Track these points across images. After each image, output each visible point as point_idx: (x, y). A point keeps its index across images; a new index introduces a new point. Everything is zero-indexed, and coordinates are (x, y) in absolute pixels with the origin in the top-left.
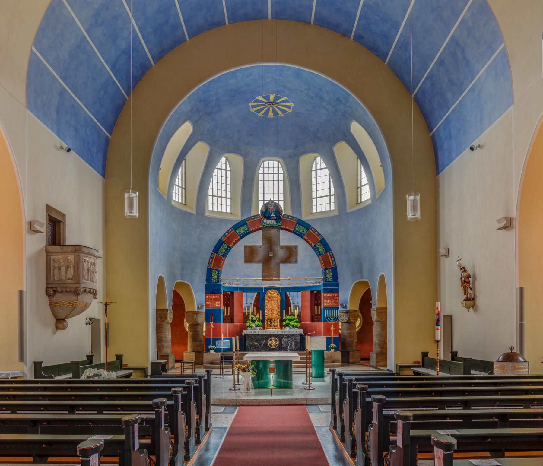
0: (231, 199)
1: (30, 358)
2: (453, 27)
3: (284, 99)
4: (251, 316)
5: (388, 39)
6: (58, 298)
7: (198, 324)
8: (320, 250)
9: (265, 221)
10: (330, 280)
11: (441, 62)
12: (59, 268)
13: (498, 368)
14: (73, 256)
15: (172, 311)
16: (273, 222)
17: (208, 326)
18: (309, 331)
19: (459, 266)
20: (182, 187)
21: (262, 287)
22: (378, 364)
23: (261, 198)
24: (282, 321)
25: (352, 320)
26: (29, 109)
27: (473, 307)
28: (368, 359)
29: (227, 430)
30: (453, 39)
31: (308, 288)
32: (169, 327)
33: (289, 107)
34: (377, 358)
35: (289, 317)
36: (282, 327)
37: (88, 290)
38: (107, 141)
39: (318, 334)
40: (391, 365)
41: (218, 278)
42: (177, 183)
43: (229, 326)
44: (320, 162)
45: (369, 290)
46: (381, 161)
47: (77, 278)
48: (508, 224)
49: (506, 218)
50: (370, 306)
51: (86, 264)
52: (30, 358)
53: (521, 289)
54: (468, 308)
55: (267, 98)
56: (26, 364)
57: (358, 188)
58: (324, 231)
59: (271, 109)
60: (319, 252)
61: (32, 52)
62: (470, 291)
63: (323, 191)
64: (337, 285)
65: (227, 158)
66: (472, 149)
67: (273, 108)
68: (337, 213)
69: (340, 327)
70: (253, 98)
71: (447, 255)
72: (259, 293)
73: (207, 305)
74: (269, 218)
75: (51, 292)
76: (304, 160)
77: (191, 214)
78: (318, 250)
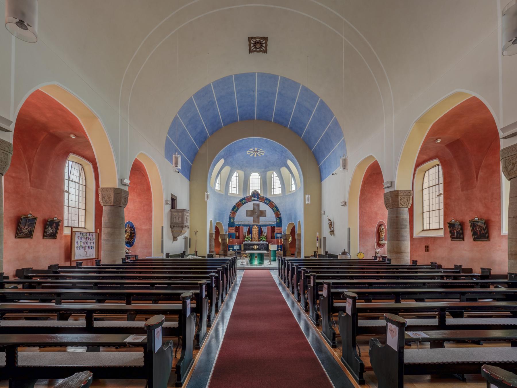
0: (238, 188)
1: (165, 252)
2: (326, 128)
3: (261, 150)
4: (246, 236)
5: (302, 129)
6: (175, 228)
7: (225, 239)
8: (275, 210)
9: (253, 198)
10: (279, 222)
11: (322, 140)
12: (176, 218)
13: (340, 257)
14: (181, 213)
15: (215, 234)
16: (256, 199)
17: (229, 240)
18: (269, 242)
19: (328, 218)
20: (219, 184)
21: (251, 224)
22: (298, 256)
23: (251, 188)
24: (259, 238)
25: (287, 238)
26: (166, 158)
27: (333, 234)
28: (294, 255)
29: (242, 277)
30: (326, 132)
31: (270, 225)
32: (214, 240)
33: (263, 153)
34: (297, 254)
35: (262, 237)
36: (259, 241)
37: (186, 226)
38: (191, 166)
39: (274, 244)
40: (303, 257)
41: (234, 221)
42: (217, 182)
43: (237, 240)
44: (275, 174)
45: (294, 227)
46: (299, 176)
47: (182, 222)
48: (345, 204)
49: (344, 202)
50: (295, 233)
51: (186, 216)
52: (165, 252)
53: (349, 228)
54: (331, 235)
55: (254, 149)
56: (164, 254)
57: (290, 185)
58: (276, 202)
59: (256, 153)
60: (274, 211)
61: (167, 137)
62: (332, 228)
63: (276, 186)
64: (282, 224)
65: (237, 172)
66: (333, 174)
67: (257, 154)
68: (282, 195)
69: (283, 241)
70: (248, 149)
71: (324, 214)
72: (250, 227)
73: (229, 232)
74: (254, 197)
75: (172, 227)
76: (268, 173)
77: (223, 195)
78: (274, 210)
